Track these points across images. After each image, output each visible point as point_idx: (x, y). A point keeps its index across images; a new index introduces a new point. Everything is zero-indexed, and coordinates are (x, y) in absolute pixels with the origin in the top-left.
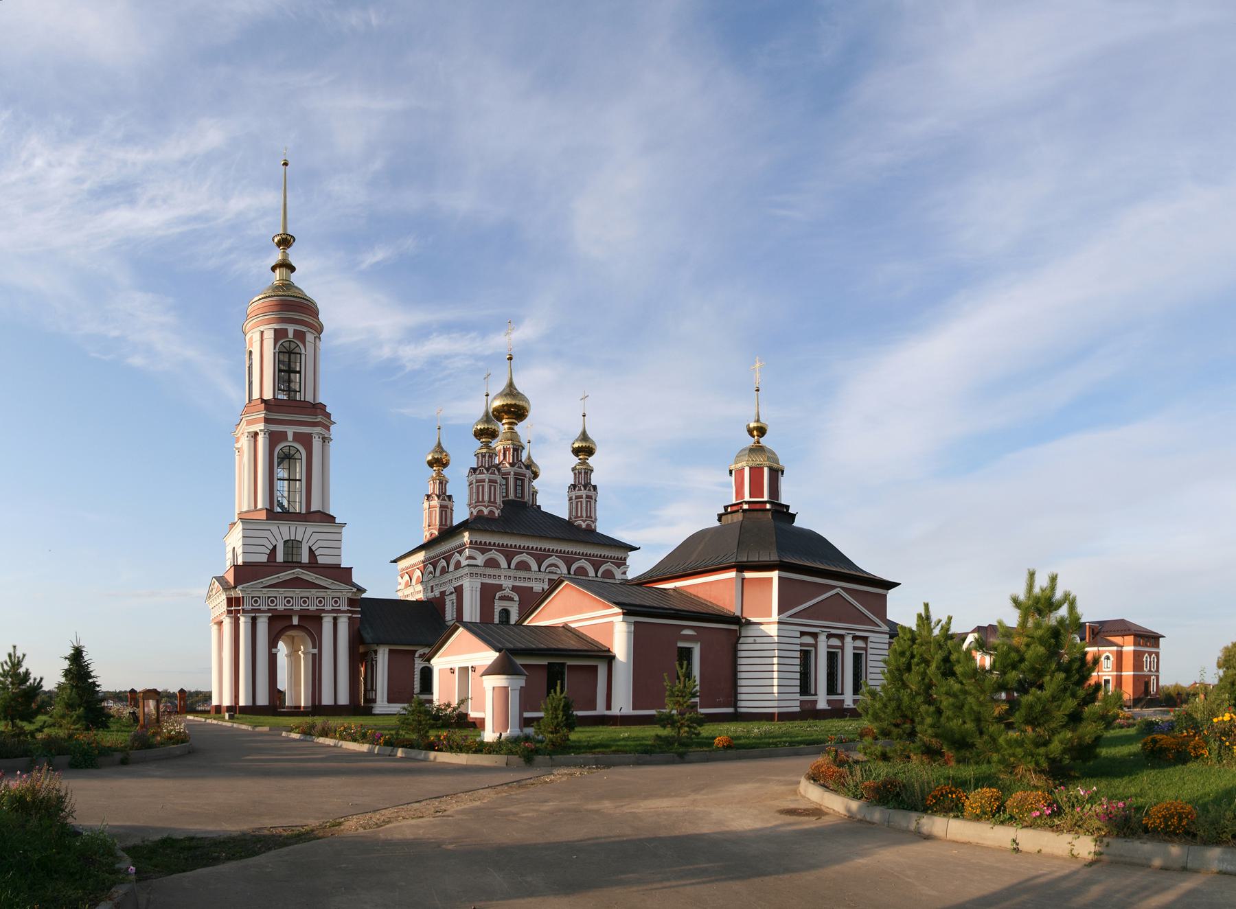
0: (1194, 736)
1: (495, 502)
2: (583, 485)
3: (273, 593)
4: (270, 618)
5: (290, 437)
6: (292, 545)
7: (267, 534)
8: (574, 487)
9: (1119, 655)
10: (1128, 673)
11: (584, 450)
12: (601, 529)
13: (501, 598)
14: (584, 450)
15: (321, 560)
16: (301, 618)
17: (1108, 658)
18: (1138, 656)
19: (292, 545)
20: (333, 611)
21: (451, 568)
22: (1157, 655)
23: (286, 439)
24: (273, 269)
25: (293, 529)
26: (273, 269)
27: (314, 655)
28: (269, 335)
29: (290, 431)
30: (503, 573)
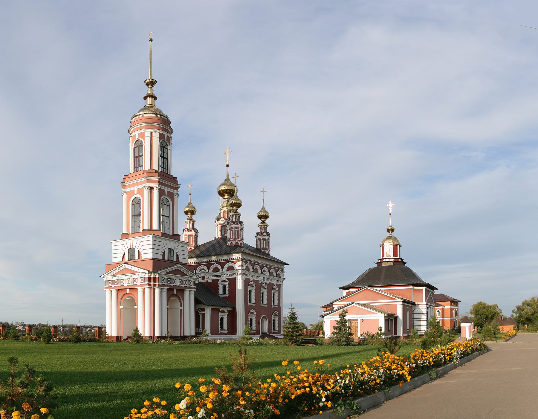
0: (340, 376)
1: (238, 238)
2: (263, 234)
4: (168, 289)
7: (122, 247)
9: (443, 310)
10: (448, 318)
11: (264, 217)
12: (273, 253)
14: (264, 217)
15: (181, 261)
16: (178, 290)
17: (438, 311)
18: (451, 310)
22: (458, 309)
23: (165, 194)
24: (145, 98)
26: (145, 98)
27: (181, 310)
28: (156, 135)
29: (167, 190)
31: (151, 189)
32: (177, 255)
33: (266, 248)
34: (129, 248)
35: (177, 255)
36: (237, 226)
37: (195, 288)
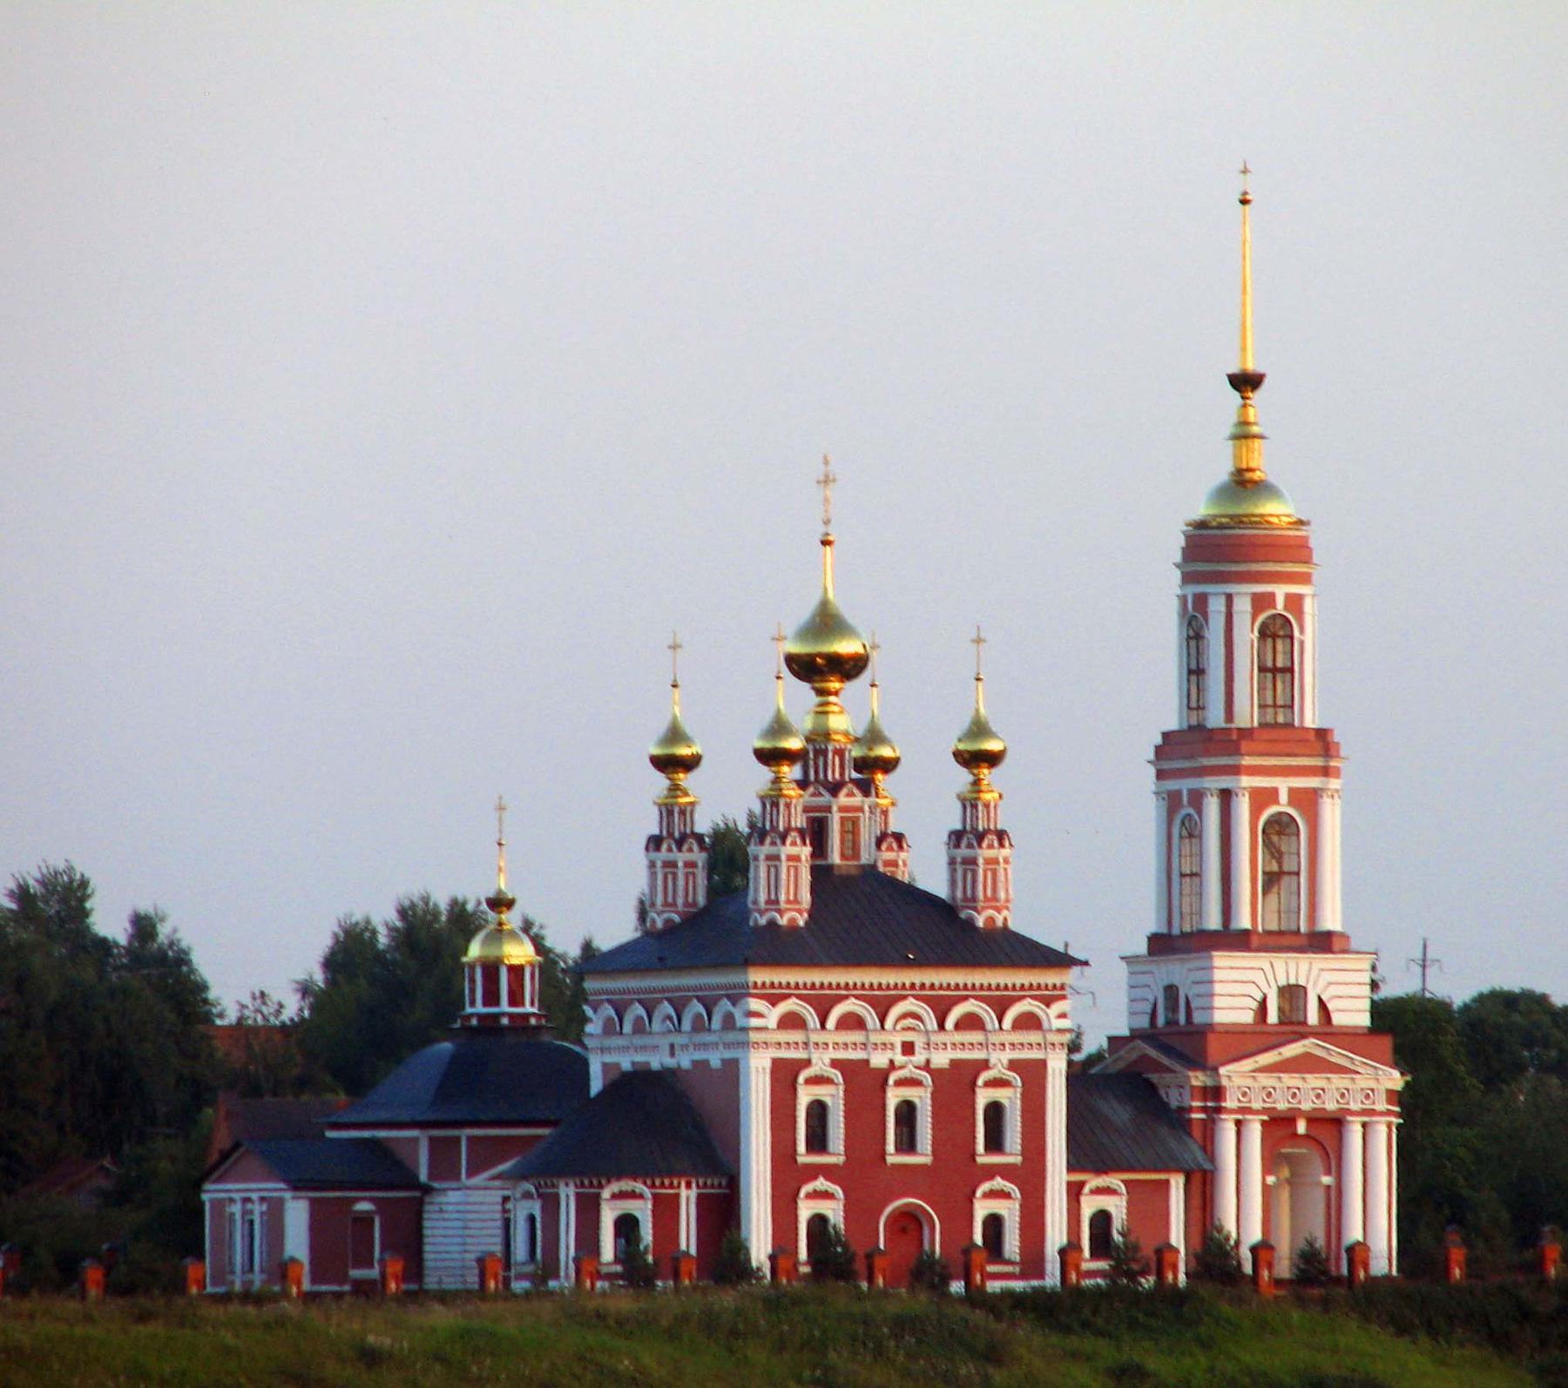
3: (1267, 1080)
4: (1264, 1123)
5: (1283, 797)
6: (1292, 994)
8: (655, 842)
13: (988, 1084)
15: (1338, 1019)
19: (1292, 994)
20: (1364, 1112)
21: (717, 1023)
25: (1292, 965)
29: (1283, 785)
30: (996, 1038)
31: (1226, 796)
32: (1322, 1005)
33: (995, 898)
34: (1282, 982)
35: (1322, 1005)
36: (991, 853)
37: (1389, 1113)
